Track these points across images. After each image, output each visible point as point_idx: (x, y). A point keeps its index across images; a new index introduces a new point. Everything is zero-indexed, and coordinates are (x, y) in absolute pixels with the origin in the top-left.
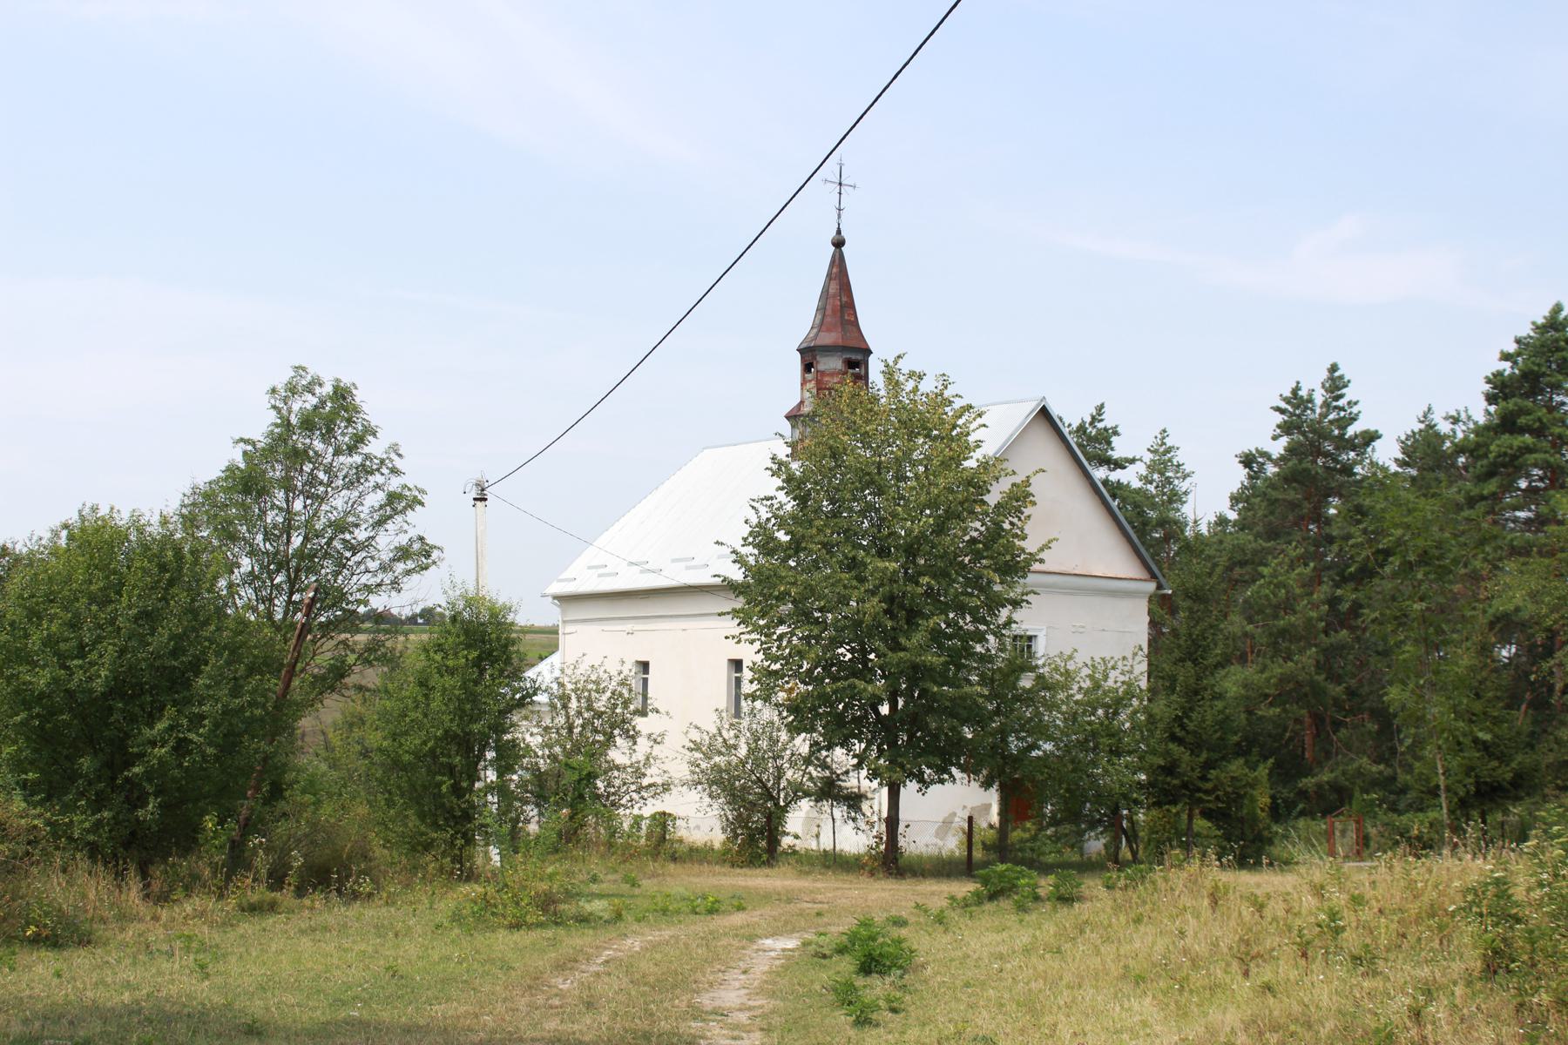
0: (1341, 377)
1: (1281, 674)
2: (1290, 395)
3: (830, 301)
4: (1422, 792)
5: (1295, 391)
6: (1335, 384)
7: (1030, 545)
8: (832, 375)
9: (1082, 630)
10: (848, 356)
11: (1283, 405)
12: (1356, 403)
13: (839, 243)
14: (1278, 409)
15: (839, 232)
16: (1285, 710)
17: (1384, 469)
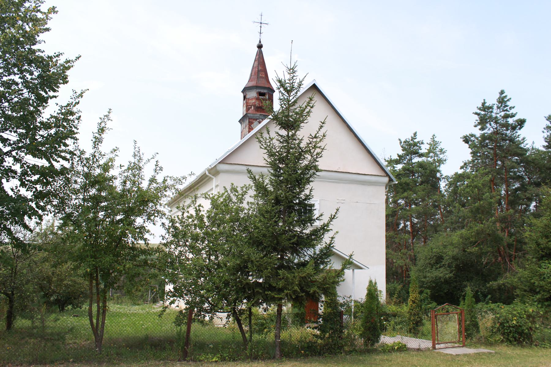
0: (506, 97)
1: (477, 230)
2: (481, 106)
3: (254, 69)
4: (525, 291)
5: (483, 104)
6: (502, 101)
7: (38, 39)
8: (252, 99)
9: (343, 202)
10: (259, 91)
11: (479, 111)
12: (513, 108)
13: (260, 47)
14: (476, 114)
15: (260, 42)
16: (481, 249)
17: (538, 150)
